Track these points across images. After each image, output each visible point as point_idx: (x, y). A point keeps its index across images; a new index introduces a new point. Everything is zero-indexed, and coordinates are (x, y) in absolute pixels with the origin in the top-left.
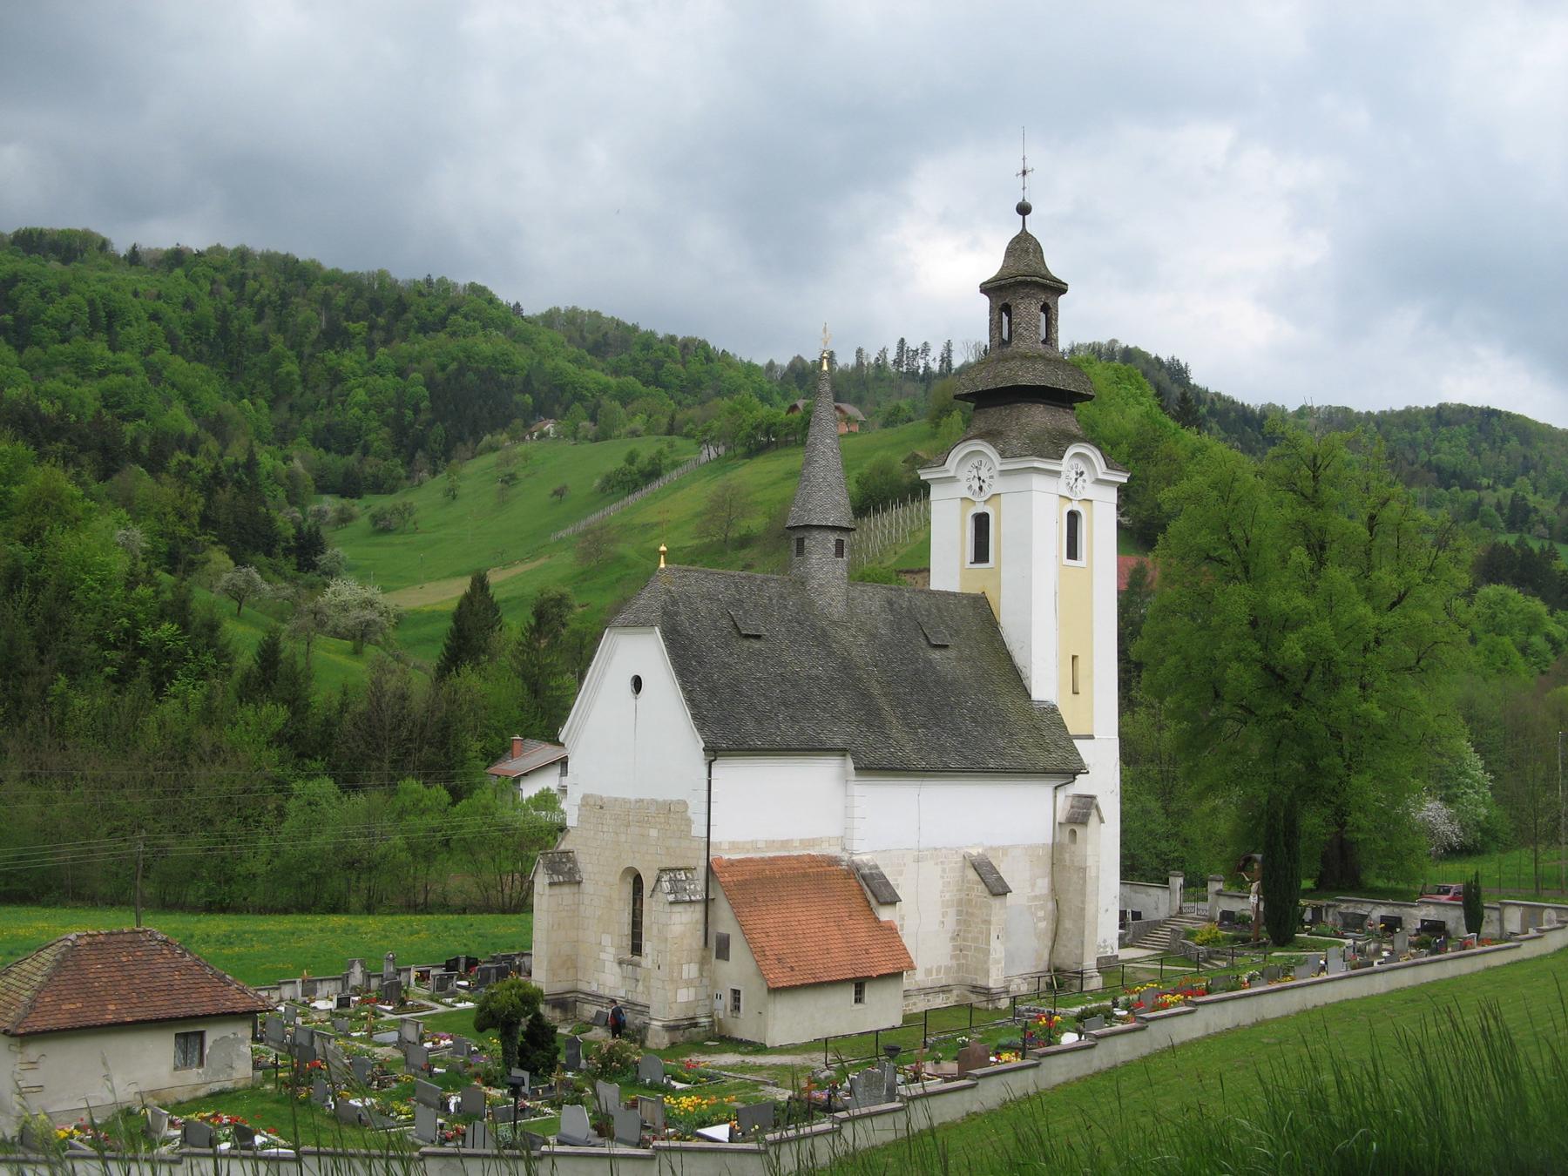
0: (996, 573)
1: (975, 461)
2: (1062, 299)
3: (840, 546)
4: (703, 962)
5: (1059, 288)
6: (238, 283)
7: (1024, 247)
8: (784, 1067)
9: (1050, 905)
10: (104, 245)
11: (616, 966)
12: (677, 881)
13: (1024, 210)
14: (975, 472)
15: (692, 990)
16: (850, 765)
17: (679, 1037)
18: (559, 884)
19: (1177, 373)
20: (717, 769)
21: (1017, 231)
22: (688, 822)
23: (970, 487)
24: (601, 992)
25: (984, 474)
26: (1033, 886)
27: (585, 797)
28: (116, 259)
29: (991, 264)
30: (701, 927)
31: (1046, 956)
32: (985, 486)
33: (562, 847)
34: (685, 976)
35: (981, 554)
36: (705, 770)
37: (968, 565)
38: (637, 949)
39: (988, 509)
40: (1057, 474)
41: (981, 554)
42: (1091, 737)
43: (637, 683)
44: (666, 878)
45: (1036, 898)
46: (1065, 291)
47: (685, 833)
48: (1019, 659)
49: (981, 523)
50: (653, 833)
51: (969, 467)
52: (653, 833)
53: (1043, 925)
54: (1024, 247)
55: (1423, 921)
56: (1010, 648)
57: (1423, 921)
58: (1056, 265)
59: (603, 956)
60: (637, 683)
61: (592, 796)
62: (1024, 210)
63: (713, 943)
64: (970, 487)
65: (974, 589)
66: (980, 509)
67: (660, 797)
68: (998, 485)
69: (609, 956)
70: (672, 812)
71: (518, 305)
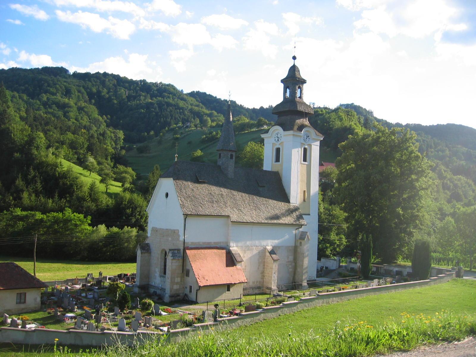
2: (305, 85)
3: (232, 156)
4: (182, 277)
5: (304, 82)
6: (103, 83)
7: (293, 69)
8: (381, 285)
9: (293, 264)
10: (66, 71)
11: (159, 277)
12: (174, 253)
13: (294, 58)
14: (277, 135)
15: (178, 286)
17: (173, 299)
18: (144, 253)
19: (118, 76)
21: (292, 65)
22: (179, 236)
24: (155, 285)
26: (288, 258)
27: (153, 228)
28: (70, 75)
30: (181, 267)
31: (292, 279)
32: (279, 139)
33: (146, 242)
34: (176, 281)
35: (278, 159)
36: (183, 221)
37: (274, 163)
38: (165, 273)
39: (280, 147)
40: (300, 136)
41: (278, 159)
42: (309, 215)
43: (167, 195)
44: (171, 252)
45: (289, 262)
46: (305, 83)
47: (178, 239)
48: (287, 191)
49: (278, 151)
50: (170, 239)
53: (291, 270)
54: (293, 69)
55: (408, 272)
57: (408, 272)
58: (303, 75)
59: (156, 275)
60: (167, 195)
61: (154, 227)
63: (185, 272)
64: (275, 140)
65: (275, 170)
66: (277, 146)
67: (172, 228)
69: (157, 274)
70: (175, 232)
71: (182, 90)
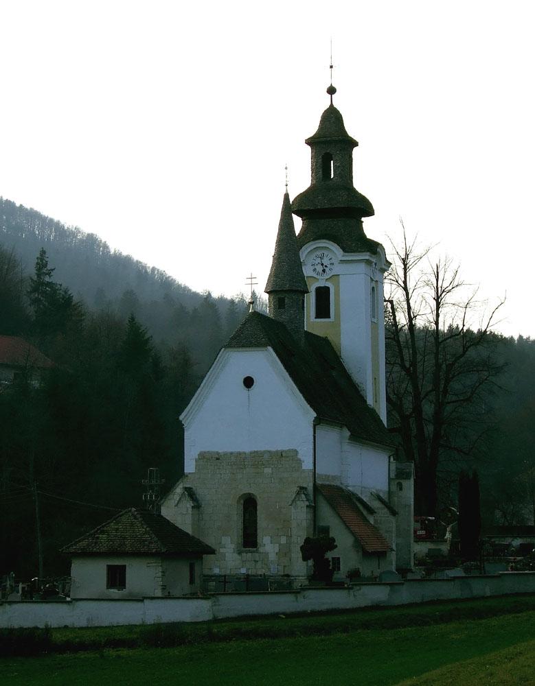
0: (337, 324)
1: (319, 253)
7: (332, 118)
11: (236, 555)
13: (332, 91)
16: (347, 433)
20: (317, 427)
22: (300, 462)
23: (315, 270)
25: (326, 261)
29: (312, 128)
32: (327, 269)
39: (328, 284)
43: (249, 382)
51: (313, 256)
52: (268, 471)
54: (332, 118)
56: (350, 372)
60: (249, 382)
62: (332, 91)
64: (315, 270)
66: (321, 284)
67: (273, 448)
68: (338, 269)
